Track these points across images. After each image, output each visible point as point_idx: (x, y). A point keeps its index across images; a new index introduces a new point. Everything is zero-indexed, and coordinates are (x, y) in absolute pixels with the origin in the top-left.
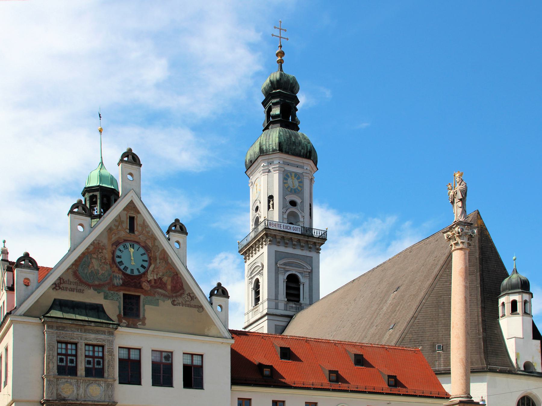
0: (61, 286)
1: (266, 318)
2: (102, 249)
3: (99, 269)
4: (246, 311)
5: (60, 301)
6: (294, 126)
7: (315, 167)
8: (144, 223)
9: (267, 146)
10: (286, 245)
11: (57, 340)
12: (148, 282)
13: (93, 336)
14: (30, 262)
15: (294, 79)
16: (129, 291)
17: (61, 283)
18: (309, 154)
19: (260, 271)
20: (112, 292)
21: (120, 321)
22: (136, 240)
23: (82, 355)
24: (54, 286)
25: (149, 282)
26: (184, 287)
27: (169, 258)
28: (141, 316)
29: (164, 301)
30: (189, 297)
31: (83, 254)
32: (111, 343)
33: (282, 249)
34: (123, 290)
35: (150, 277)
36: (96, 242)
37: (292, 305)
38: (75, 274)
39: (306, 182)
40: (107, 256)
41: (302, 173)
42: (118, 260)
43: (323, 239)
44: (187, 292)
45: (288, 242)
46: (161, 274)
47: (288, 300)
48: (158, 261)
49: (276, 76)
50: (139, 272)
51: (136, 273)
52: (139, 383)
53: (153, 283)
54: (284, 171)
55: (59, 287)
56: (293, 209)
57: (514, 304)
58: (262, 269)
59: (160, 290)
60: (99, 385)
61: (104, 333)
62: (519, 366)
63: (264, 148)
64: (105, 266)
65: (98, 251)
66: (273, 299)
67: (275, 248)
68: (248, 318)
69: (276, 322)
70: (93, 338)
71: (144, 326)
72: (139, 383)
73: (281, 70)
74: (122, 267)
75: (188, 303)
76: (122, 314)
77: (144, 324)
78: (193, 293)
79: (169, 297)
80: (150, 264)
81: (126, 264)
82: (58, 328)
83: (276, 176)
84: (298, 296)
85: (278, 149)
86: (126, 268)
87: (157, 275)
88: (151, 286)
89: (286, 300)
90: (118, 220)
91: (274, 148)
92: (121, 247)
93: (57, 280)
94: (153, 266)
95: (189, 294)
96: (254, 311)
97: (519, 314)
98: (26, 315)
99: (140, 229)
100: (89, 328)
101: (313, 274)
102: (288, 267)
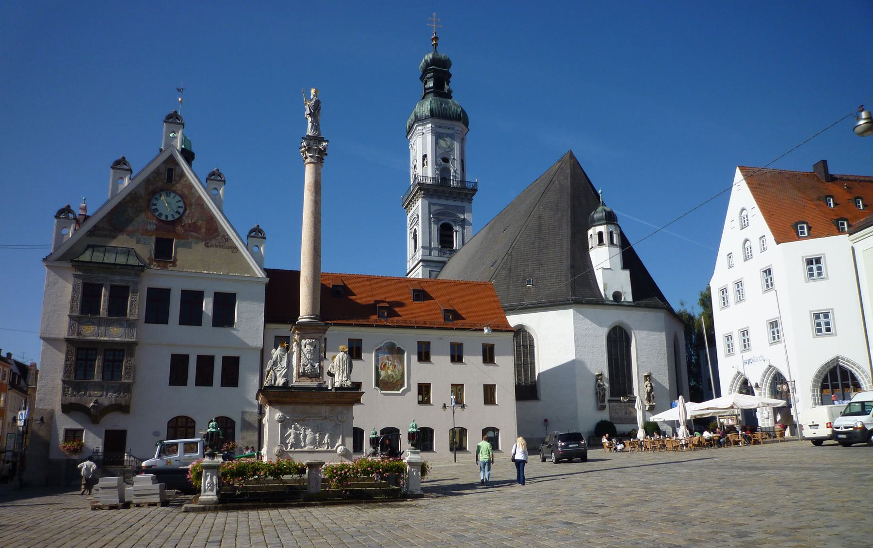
1: (421, 264)
9: (421, 113)
13: (118, 278)
18: (462, 118)
19: (417, 221)
24: (89, 233)
26: (219, 230)
30: (223, 239)
31: (120, 203)
33: (435, 201)
36: (133, 192)
37: (446, 250)
44: (221, 235)
45: (464, 197)
46: (195, 218)
48: (193, 207)
50: (174, 217)
51: (170, 218)
53: (187, 227)
57: (600, 234)
58: (418, 220)
59: (193, 234)
62: (608, 297)
63: (419, 114)
66: (428, 248)
73: (436, 51)
75: (222, 244)
81: (161, 211)
83: (429, 138)
85: (430, 115)
86: (161, 214)
87: (191, 219)
91: (427, 114)
93: (93, 227)
95: (224, 236)
96: (414, 258)
97: (605, 245)
102: (440, 217)
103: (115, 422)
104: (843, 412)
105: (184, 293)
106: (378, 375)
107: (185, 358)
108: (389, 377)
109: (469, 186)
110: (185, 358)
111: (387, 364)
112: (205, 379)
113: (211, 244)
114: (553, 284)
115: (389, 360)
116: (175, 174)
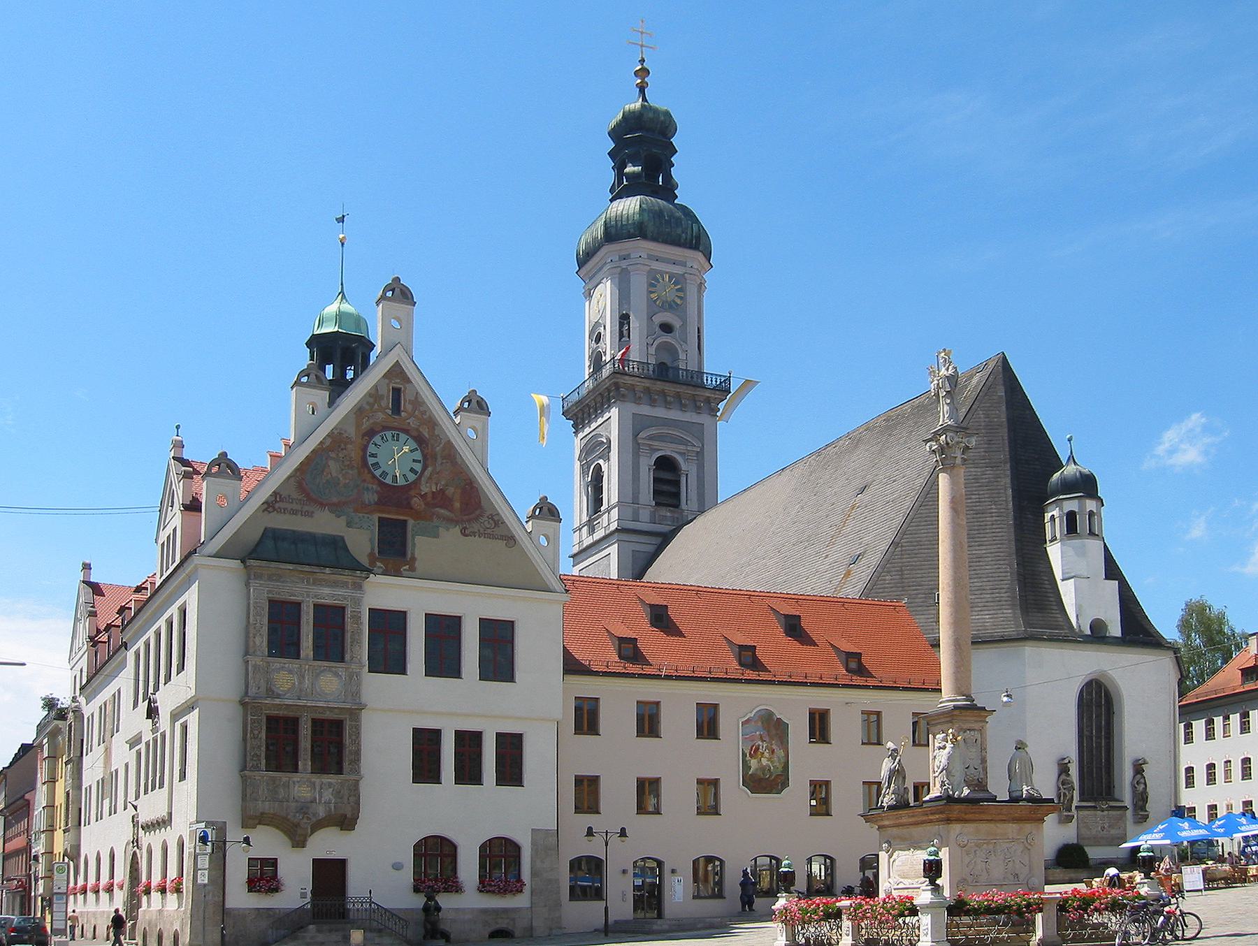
0: (277, 505)
2: (346, 444)
3: (340, 476)
4: (577, 524)
5: (274, 531)
6: (668, 191)
7: (707, 263)
8: (416, 398)
10: (652, 403)
11: (268, 597)
12: (422, 496)
13: (327, 591)
14: (228, 466)
15: (667, 114)
16: (389, 513)
17: (276, 502)
20: (361, 515)
21: (372, 563)
22: (404, 427)
23: (308, 622)
24: (266, 506)
25: (424, 497)
27: (458, 456)
28: (409, 555)
29: (448, 529)
30: (491, 521)
32: (358, 602)
33: (645, 410)
34: (380, 511)
35: (425, 489)
36: (336, 432)
38: (301, 487)
39: (691, 290)
40: (353, 455)
41: (683, 275)
42: (371, 461)
43: (723, 389)
44: (488, 513)
47: (657, 504)
48: (439, 460)
49: (637, 105)
52: (403, 671)
54: (649, 272)
55: (274, 508)
56: (667, 338)
57: (1071, 517)
60: (336, 674)
61: (344, 585)
63: (613, 231)
64: (350, 472)
65: (339, 446)
66: (628, 501)
67: (633, 408)
68: (580, 536)
69: (637, 545)
70: (328, 595)
71: (412, 572)
72: (403, 671)
74: (378, 473)
75: (489, 531)
76: (376, 551)
77: (412, 569)
78: (498, 514)
79: (456, 522)
80: (424, 469)
82: (270, 578)
84: (677, 495)
87: (437, 484)
88: (427, 504)
89: (654, 503)
90: (374, 395)
92: (377, 439)
94: (430, 469)
95: (491, 517)
98: (217, 555)
99: (409, 407)
100: (321, 576)
101: (704, 456)
102: (656, 443)
103: (327, 844)
104: (1072, 753)
105: (499, 736)
106: (746, 765)
107: (436, 734)
108: (764, 770)
109: (709, 382)
110: (436, 734)
111: (761, 747)
112: (468, 772)
113: (471, 530)
114: (987, 604)
115: (763, 741)
116: (405, 399)
